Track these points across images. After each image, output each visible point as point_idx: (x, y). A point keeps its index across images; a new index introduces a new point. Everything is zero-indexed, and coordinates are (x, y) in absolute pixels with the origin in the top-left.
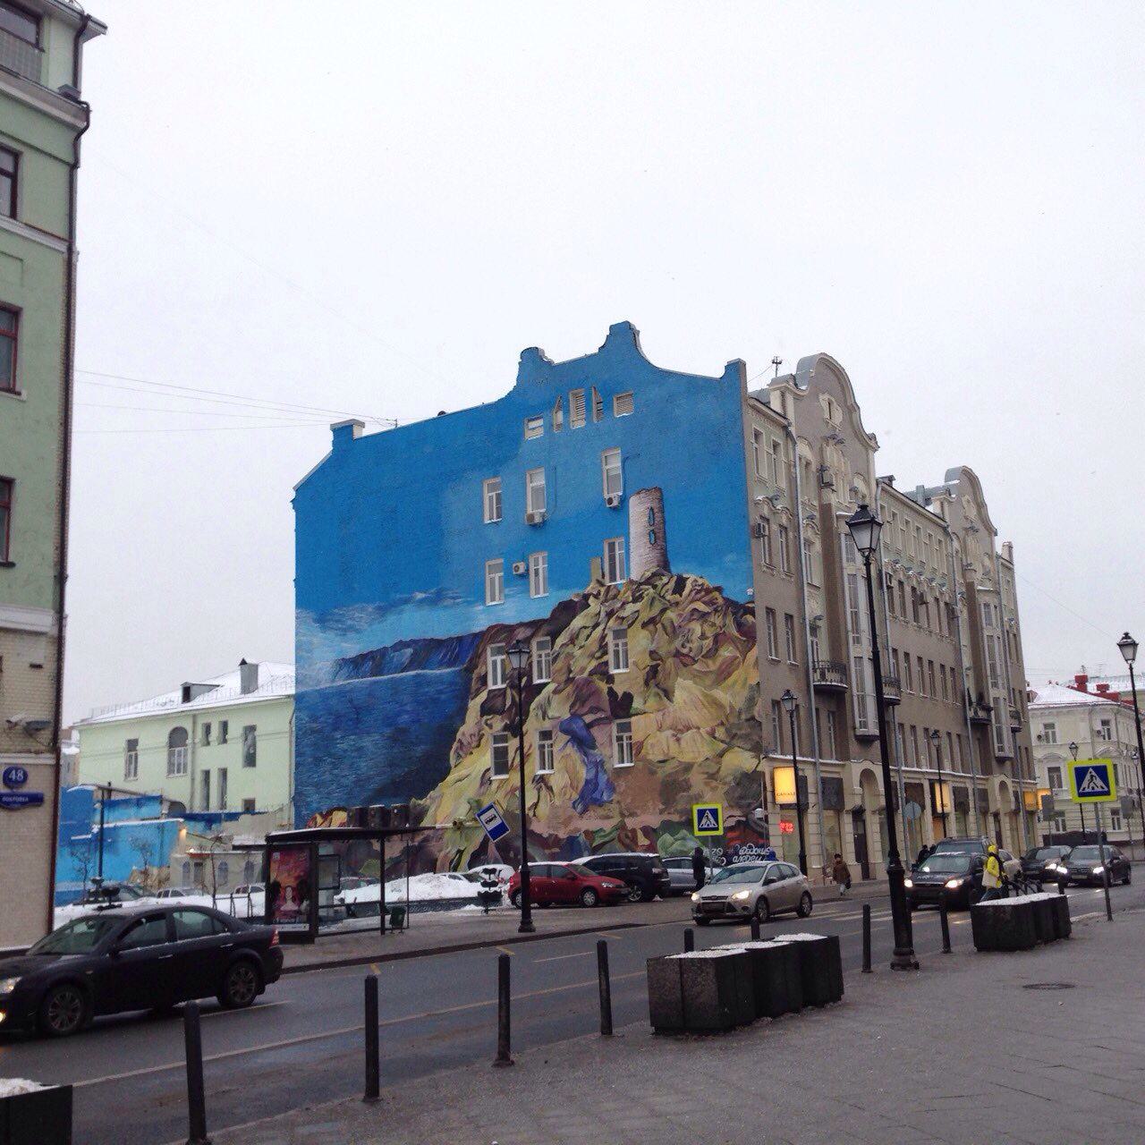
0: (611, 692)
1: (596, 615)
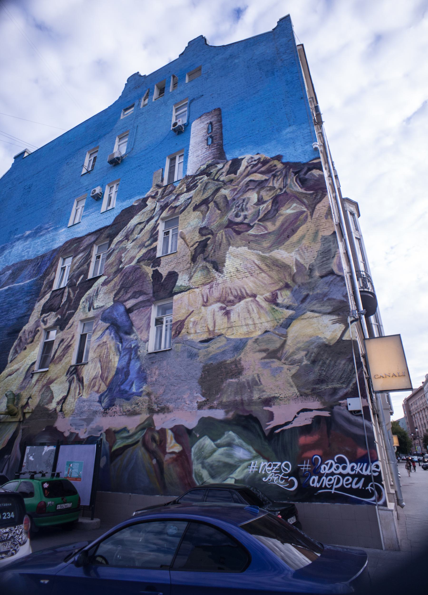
0: (157, 275)
1: (152, 210)
